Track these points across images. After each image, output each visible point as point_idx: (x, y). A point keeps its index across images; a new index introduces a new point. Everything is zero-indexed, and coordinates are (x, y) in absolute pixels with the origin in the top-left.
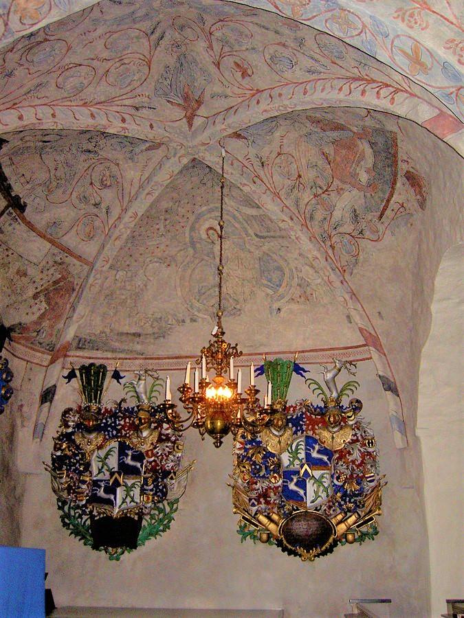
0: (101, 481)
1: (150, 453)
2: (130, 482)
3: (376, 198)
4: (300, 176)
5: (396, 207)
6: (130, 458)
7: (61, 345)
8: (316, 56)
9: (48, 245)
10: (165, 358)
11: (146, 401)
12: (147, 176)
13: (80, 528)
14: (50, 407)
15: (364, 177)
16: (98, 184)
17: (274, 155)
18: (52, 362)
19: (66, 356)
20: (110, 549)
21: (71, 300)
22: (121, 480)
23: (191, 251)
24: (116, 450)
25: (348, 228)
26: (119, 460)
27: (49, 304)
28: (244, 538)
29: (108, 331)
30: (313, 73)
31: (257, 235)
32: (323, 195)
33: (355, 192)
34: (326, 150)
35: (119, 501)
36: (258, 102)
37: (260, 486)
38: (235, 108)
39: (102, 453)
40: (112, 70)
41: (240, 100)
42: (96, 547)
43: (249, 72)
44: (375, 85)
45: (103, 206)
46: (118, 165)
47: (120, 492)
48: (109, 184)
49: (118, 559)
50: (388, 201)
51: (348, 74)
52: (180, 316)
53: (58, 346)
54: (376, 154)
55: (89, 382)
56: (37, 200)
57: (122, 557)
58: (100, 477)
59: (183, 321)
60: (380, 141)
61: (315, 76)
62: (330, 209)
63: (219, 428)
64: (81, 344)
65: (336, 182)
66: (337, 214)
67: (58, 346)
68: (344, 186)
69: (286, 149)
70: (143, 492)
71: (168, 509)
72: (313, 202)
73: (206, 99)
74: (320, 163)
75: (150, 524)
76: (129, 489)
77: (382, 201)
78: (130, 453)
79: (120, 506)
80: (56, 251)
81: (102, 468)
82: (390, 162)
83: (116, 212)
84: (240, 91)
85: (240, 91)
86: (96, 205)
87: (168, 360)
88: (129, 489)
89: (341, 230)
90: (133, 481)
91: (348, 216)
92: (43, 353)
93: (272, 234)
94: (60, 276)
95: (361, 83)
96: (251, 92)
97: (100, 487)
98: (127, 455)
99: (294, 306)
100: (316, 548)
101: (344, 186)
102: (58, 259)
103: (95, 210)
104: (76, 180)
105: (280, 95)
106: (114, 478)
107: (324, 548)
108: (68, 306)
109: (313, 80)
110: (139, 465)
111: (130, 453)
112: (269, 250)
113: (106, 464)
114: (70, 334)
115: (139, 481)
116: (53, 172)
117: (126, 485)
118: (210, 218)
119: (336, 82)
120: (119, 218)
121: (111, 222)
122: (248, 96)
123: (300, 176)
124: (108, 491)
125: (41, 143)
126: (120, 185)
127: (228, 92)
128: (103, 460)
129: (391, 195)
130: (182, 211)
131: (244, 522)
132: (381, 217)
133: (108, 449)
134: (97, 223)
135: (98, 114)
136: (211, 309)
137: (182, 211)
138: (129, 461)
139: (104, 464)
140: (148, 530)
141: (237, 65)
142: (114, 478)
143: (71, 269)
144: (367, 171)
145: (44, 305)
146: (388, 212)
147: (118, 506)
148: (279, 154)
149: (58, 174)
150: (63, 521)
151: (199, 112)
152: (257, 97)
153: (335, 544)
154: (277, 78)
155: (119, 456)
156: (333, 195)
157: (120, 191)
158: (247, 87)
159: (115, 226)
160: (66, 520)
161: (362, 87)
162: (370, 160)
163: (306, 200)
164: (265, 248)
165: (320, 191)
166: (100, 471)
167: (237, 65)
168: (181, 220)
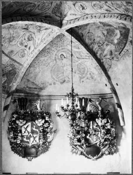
0: (25, 135)
1: (42, 126)
2: (35, 136)
3: (119, 48)
4: (94, 40)
5: (125, 51)
6: (34, 128)
7: (11, 91)
8: (110, 6)
9: (8, 59)
10: (45, 96)
11: (39, 109)
12: (44, 37)
13: (18, 151)
14: (7, 112)
15: (116, 41)
16: (27, 39)
17: (87, 33)
18: (8, 97)
19: (13, 95)
20: (28, 157)
21: (15, 77)
22: (32, 135)
23: (55, 62)
24: (30, 126)
25: (108, 57)
26: (31, 128)
27: (7, 78)
28: (73, 153)
29: (26, 87)
30: (108, 11)
31: (77, 57)
32: (102, 46)
33: (112, 45)
34: (104, 32)
35: (31, 142)
36: (87, 18)
37: (79, 137)
38: (78, 19)
39: (25, 126)
40: (41, 5)
41: (80, 16)
42: (24, 157)
43: (85, 8)
44: (129, 17)
45: (28, 47)
46: (34, 34)
47: (32, 139)
48: (30, 40)
49: (31, 160)
50: (123, 49)
51: (121, 13)
52: (50, 83)
53: (10, 92)
54: (121, 34)
55: (21, 104)
56: (6, 44)
57: (32, 160)
58: (25, 134)
59: (51, 84)
60: (123, 31)
61: (109, 12)
62: (103, 50)
63: (17, 121)
64: (17, 91)
65: (106, 42)
66: (105, 52)
67: (10, 92)
68: (108, 43)
69: (90, 31)
70: (39, 139)
71: (48, 144)
72: (98, 48)
73: (68, 15)
74: (101, 36)
75: (41, 149)
76: (34, 138)
77: (121, 49)
78: (35, 126)
79: (31, 144)
80: (11, 61)
81: (25, 131)
82: (125, 37)
83: (32, 48)
84: (81, 14)
85: (81, 14)
86: (26, 46)
87: (46, 97)
88: (34, 138)
89: (106, 57)
90: (36, 135)
91: (109, 54)
92: (5, 94)
93: (83, 57)
94: (11, 69)
95: (124, 16)
96: (84, 14)
97: (25, 137)
98: (34, 127)
99: (88, 80)
100: (96, 156)
101: (108, 43)
102: (11, 63)
103: (25, 48)
104: (19, 38)
105: (95, 16)
106: (29, 134)
107: (99, 156)
108: (14, 79)
109: (108, 13)
110: (37, 130)
111: (35, 126)
112: (81, 62)
113: (27, 130)
114: (14, 89)
115: (38, 136)
116: (12, 35)
117: (33, 137)
118: (62, 51)
119: (116, 14)
120: (33, 51)
121: (30, 52)
122: (83, 15)
123: (94, 40)
124: (28, 138)
125: (10, 26)
126: (34, 40)
127: (76, 13)
128: (26, 129)
129: (124, 47)
130: (53, 49)
131: (73, 149)
132: (120, 54)
133: (27, 125)
134: (26, 52)
135: (35, 19)
136: (60, 81)
137: (53, 49)
138: (34, 129)
139: (26, 130)
140: (41, 151)
141: (81, 5)
142: (29, 134)
143: (15, 66)
144: (117, 39)
145: (6, 78)
146: (123, 52)
147: (31, 143)
148: (88, 33)
149: (14, 35)
150: (12, 149)
151: (65, 19)
152: (87, 16)
153: (102, 155)
154: (95, 11)
155: (31, 127)
156: (105, 46)
157: (34, 41)
158: (84, 12)
159: (32, 53)
160: (13, 149)
161: (125, 17)
162: (119, 36)
163: (96, 47)
164: (79, 62)
165: (100, 45)
166: (25, 132)
167: (81, 5)
168: (52, 52)
